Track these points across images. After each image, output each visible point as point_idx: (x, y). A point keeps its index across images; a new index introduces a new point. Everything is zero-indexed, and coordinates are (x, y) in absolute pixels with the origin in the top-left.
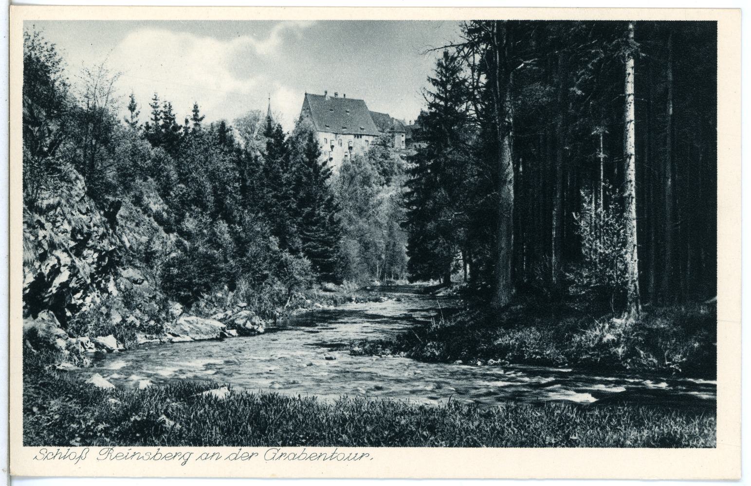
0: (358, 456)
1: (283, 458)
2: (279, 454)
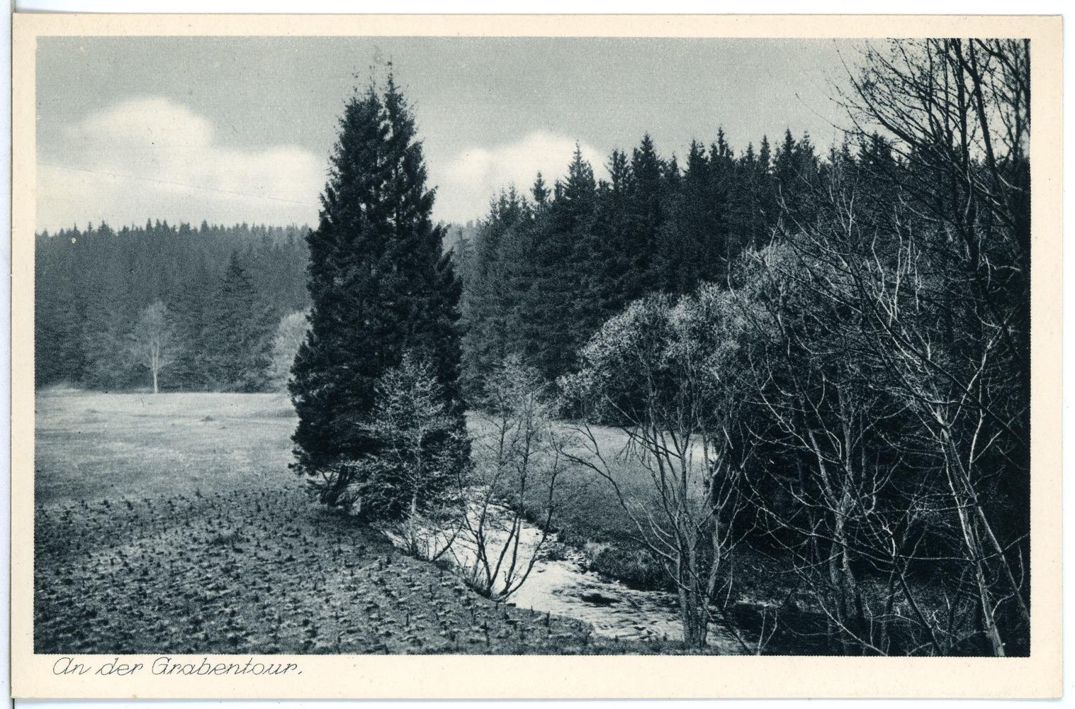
0: (281, 669)
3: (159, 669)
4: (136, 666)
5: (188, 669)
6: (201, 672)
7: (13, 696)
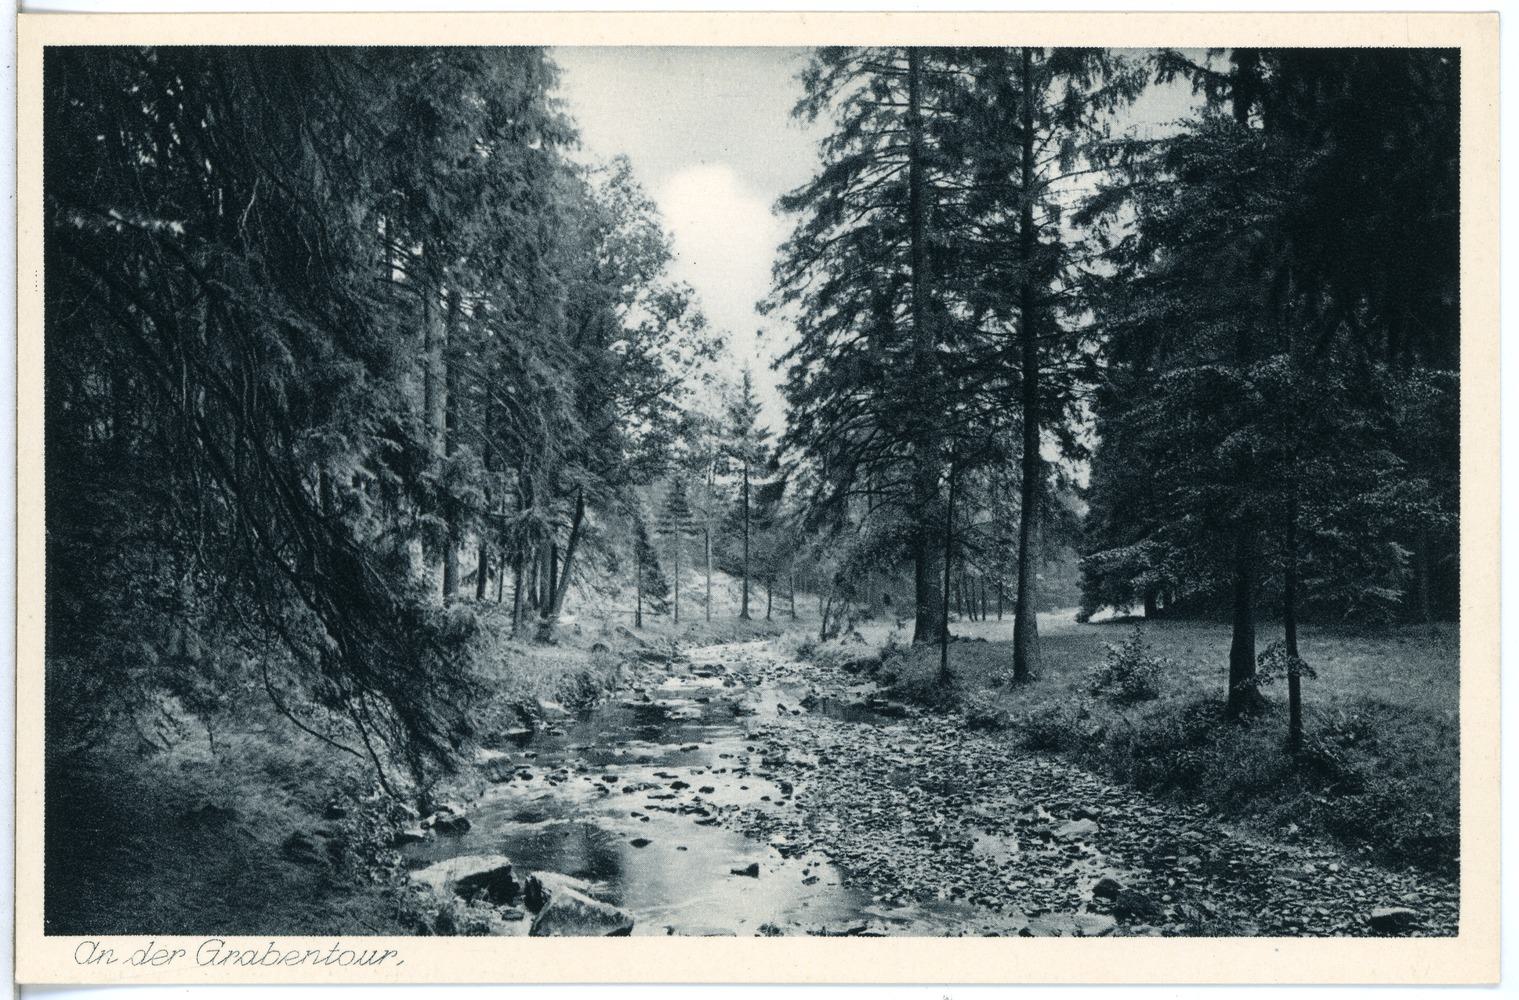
0: (377, 956)
1: (233, 959)
2: (224, 953)
3: (205, 957)
4: (388, 953)
5: (246, 959)
6: (266, 961)
7: (20, 979)
